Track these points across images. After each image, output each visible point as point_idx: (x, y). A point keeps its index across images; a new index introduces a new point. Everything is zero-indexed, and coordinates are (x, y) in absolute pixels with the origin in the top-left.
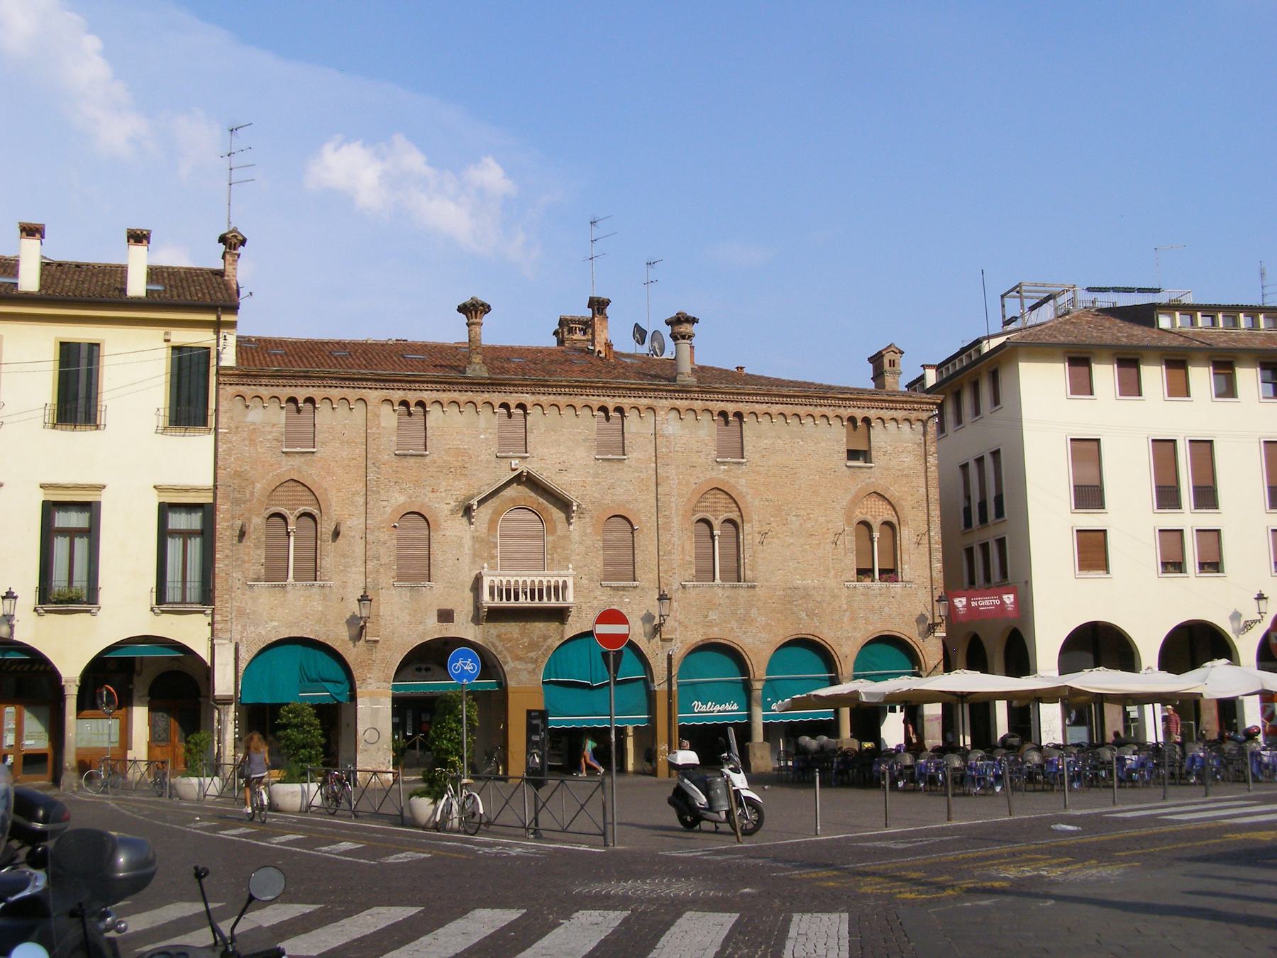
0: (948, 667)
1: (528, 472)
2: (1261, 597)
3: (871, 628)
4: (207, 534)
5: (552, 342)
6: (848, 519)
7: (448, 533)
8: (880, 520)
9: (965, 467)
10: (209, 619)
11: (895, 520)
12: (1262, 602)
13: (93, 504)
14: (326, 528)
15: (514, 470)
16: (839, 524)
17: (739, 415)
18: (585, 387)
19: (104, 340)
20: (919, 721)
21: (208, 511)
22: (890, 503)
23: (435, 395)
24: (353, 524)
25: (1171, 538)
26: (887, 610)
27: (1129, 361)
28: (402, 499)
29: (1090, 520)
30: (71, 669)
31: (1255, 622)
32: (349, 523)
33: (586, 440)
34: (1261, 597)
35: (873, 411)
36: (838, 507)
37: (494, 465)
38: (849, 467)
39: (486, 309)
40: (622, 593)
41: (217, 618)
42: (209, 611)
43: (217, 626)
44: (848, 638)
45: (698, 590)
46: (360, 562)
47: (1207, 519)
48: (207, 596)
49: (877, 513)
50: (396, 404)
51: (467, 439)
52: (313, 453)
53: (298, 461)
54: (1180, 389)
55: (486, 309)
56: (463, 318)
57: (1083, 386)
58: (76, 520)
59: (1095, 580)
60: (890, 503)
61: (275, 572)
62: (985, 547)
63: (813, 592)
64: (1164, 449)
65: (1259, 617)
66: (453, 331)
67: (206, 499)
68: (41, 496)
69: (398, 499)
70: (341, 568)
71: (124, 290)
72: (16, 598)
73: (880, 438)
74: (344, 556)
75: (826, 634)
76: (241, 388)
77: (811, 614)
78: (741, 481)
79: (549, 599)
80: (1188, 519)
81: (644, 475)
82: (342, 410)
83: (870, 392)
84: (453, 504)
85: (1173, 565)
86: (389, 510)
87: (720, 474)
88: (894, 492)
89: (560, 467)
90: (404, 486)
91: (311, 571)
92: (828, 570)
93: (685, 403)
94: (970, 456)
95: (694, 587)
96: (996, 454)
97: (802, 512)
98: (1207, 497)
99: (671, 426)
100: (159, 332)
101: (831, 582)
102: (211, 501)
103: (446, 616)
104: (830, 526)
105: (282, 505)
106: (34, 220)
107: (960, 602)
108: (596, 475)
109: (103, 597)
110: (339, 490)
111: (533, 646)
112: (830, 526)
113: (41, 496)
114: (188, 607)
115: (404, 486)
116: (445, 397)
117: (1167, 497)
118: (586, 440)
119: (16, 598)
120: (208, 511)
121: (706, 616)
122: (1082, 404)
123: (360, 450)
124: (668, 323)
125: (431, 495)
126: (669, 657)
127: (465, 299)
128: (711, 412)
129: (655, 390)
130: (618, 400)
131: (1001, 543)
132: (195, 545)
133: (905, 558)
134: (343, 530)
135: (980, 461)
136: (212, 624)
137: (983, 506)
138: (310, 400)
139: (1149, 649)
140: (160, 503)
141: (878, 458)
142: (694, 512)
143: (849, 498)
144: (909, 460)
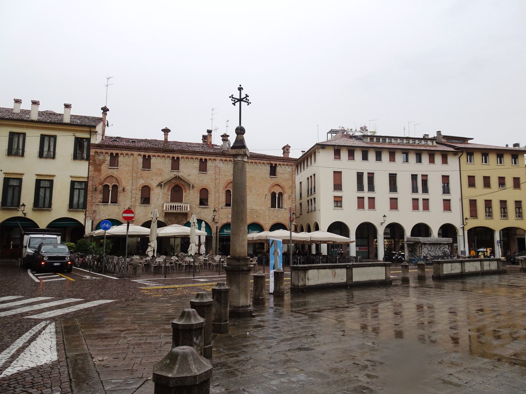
1: (179, 176)
2: (384, 216)
3: (274, 221)
5: (201, 142)
6: (269, 191)
7: (156, 192)
8: (278, 192)
9: (308, 179)
10: (85, 213)
11: (282, 192)
12: (385, 217)
14: (120, 189)
15: (175, 175)
16: (267, 192)
17: (149, 156)
18: (196, 153)
21: (86, 183)
22: (281, 187)
23: (154, 154)
24: (128, 188)
25: (415, 201)
26: (279, 216)
28: (143, 182)
29: (338, 194)
31: (383, 223)
32: (127, 188)
33: (196, 168)
34: (384, 216)
35: (278, 162)
36: (266, 188)
37: (170, 173)
38: (270, 177)
39: (169, 131)
40: (204, 209)
41: (87, 213)
42: (85, 211)
43: (87, 215)
44: (268, 223)
45: (225, 209)
46: (130, 199)
47: (415, 196)
48: (85, 207)
49: (277, 190)
50: (254, 163)
51: (162, 166)
52: (117, 168)
53: (111, 170)
55: (169, 131)
56: (163, 133)
58: (47, 184)
59: (447, 213)
60: (281, 187)
61: (105, 201)
62: (311, 200)
63: (258, 211)
65: (384, 222)
66: (161, 137)
67: (86, 180)
68: (69, 180)
69: (142, 182)
70: (124, 200)
72: (25, 206)
74: (125, 197)
75: (261, 222)
76: (97, 150)
77: (258, 217)
79: (173, 210)
80: (366, 194)
81: (212, 177)
82: (127, 157)
83: (282, 158)
84: (158, 183)
85: (415, 207)
86: (139, 185)
88: (283, 184)
89: (188, 174)
90: (144, 178)
91: (115, 201)
92: (263, 205)
93: (225, 158)
94: (309, 176)
95: (225, 208)
96: (314, 175)
97: (256, 189)
99: (221, 165)
100: (71, 134)
101: (264, 208)
102: (87, 180)
104: (264, 193)
105: (107, 182)
106: (36, 99)
108: (198, 177)
109: (53, 206)
110: (125, 179)
112: (264, 193)
113: (36, 178)
114: (78, 210)
115: (144, 178)
116: (156, 154)
118: (196, 168)
119: (25, 206)
120: (86, 183)
121: (228, 216)
122: (337, 162)
123: (131, 168)
124: (221, 136)
125: (151, 181)
126: (217, 227)
127: (164, 128)
128: (227, 161)
129: (216, 155)
130: (168, 154)
131: (315, 199)
132: (82, 192)
133: (285, 202)
134: (126, 189)
135: (311, 177)
136: (85, 215)
137: (311, 189)
140: (71, 181)
143: (270, 185)
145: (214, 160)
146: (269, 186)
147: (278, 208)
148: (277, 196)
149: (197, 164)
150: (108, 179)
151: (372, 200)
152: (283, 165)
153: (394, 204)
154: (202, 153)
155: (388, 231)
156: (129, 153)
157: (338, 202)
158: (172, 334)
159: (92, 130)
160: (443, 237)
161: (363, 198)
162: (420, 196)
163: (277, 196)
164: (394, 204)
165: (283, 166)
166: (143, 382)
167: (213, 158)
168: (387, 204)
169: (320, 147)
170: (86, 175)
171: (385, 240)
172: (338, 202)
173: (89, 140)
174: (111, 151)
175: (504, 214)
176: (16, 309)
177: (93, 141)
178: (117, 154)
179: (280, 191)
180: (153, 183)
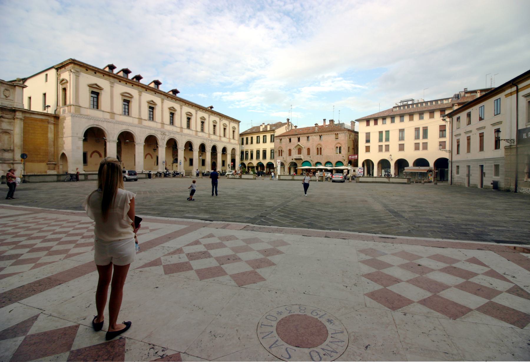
0: (313, 166)
2: (391, 155)
4: (274, 152)
13: (191, 152)
19: (87, 152)
20: (294, 170)
25: (381, 147)
27: (411, 115)
29: (368, 144)
30: (265, 165)
34: (391, 155)
49: (339, 146)
53: (280, 145)
54: (402, 121)
57: (368, 124)
64: (381, 133)
67: (273, 149)
69: (288, 148)
71: (260, 131)
73: (339, 136)
78: (322, 143)
87: (320, 142)
88: (341, 142)
98: (387, 139)
99: (315, 137)
103: (292, 159)
107: (350, 157)
111: (300, 162)
117: (381, 140)
138: (337, 134)
139: (334, 163)
141: (339, 139)
142: (317, 147)
144: (343, 138)
145: (312, 135)
146: (334, 144)
147: (320, 154)
148: (319, 149)
149: (306, 138)
150: (318, 146)
151: (387, 147)
152: (341, 133)
153: (402, 148)
154: (307, 134)
155: (380, 165)
156: (285, 137)
157: (368, 149)
158: (93, 240)
159: (274, 131)
160: (390, 168)
161: (419, 143)
162: (421, 141)
163: (319, 149)
164: (402, 148)
165: (341, 134)
166: (266, 335)
167: (311, 135)
168: (413, 147)
169: (3, 150)
170: (274, 147)
171: (390, 171)
172: (368, 149)
173: (274, 135)
174: (280, 138)
175: (258, 157)
176: (212, 221)
177: (275, 135)
178: (322, 135)
179: (340, 146)
180: (292, 148)
